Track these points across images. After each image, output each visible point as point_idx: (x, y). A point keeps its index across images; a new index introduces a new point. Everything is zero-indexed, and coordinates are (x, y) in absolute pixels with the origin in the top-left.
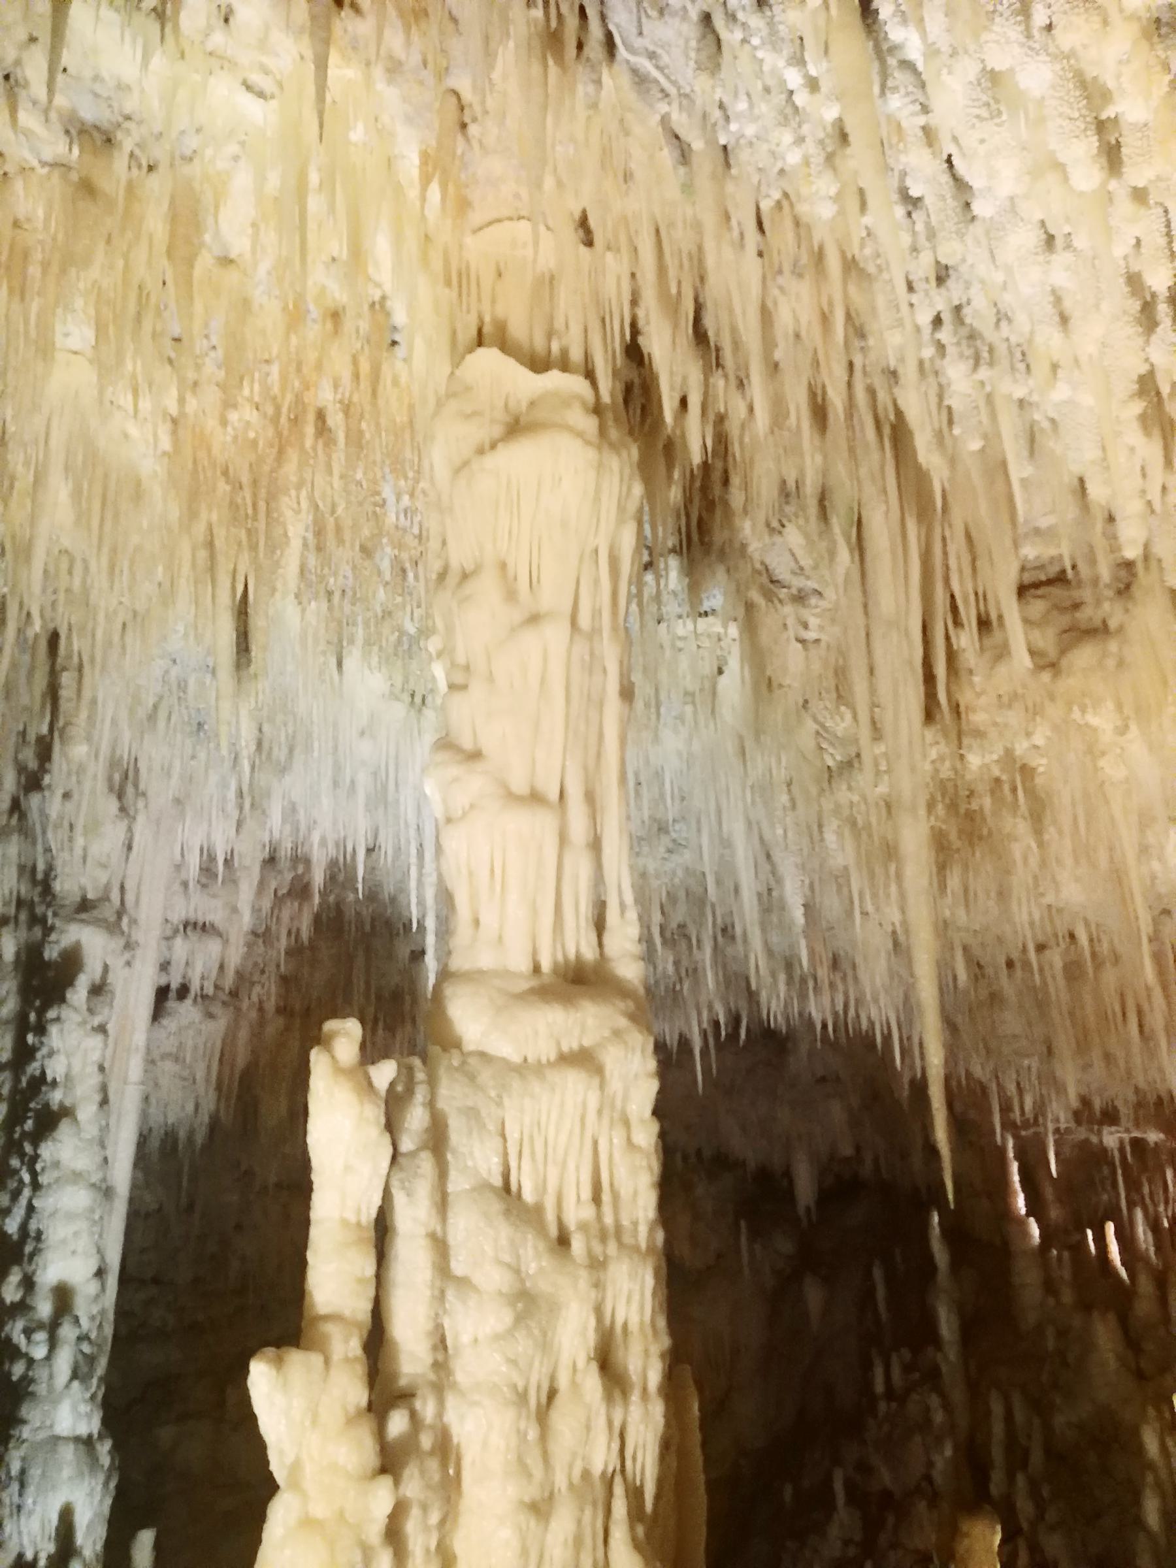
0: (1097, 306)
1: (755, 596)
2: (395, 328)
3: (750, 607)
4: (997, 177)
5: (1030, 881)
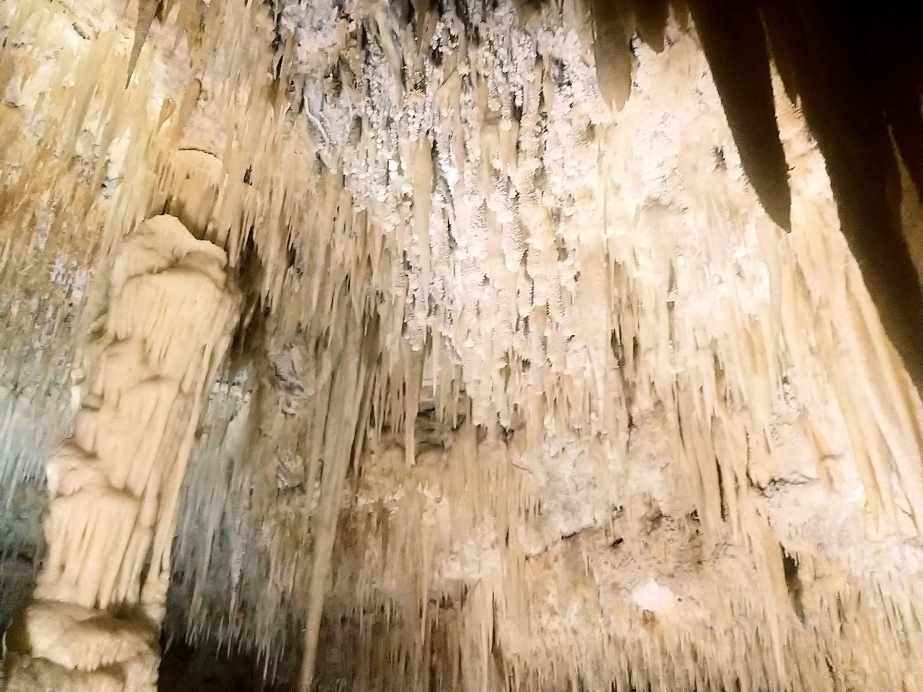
0: (496, 314)
1: (266, 381)
2: (107, 178)
3: (261, 388)
4: (473, 243)
5: (370, 573)
